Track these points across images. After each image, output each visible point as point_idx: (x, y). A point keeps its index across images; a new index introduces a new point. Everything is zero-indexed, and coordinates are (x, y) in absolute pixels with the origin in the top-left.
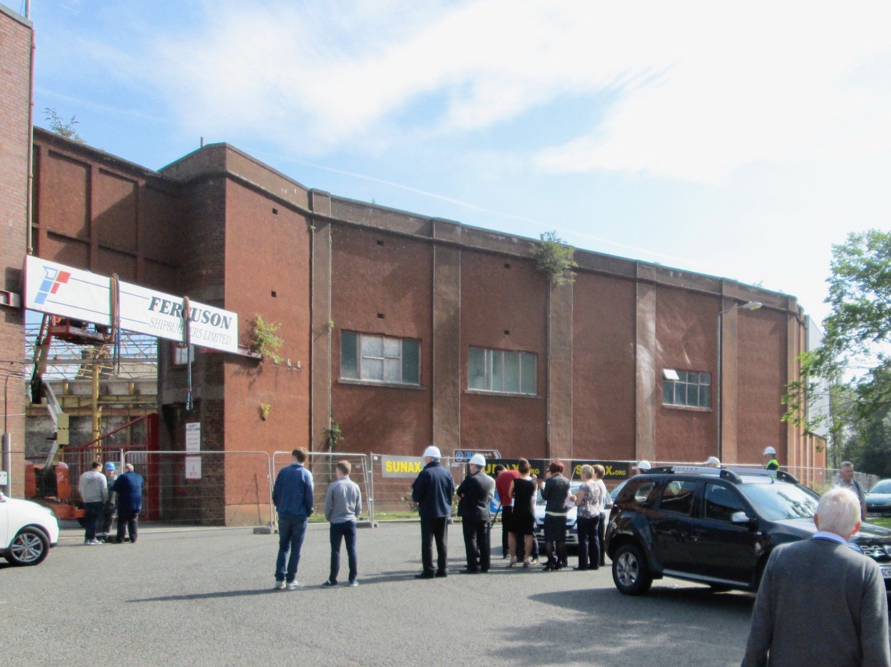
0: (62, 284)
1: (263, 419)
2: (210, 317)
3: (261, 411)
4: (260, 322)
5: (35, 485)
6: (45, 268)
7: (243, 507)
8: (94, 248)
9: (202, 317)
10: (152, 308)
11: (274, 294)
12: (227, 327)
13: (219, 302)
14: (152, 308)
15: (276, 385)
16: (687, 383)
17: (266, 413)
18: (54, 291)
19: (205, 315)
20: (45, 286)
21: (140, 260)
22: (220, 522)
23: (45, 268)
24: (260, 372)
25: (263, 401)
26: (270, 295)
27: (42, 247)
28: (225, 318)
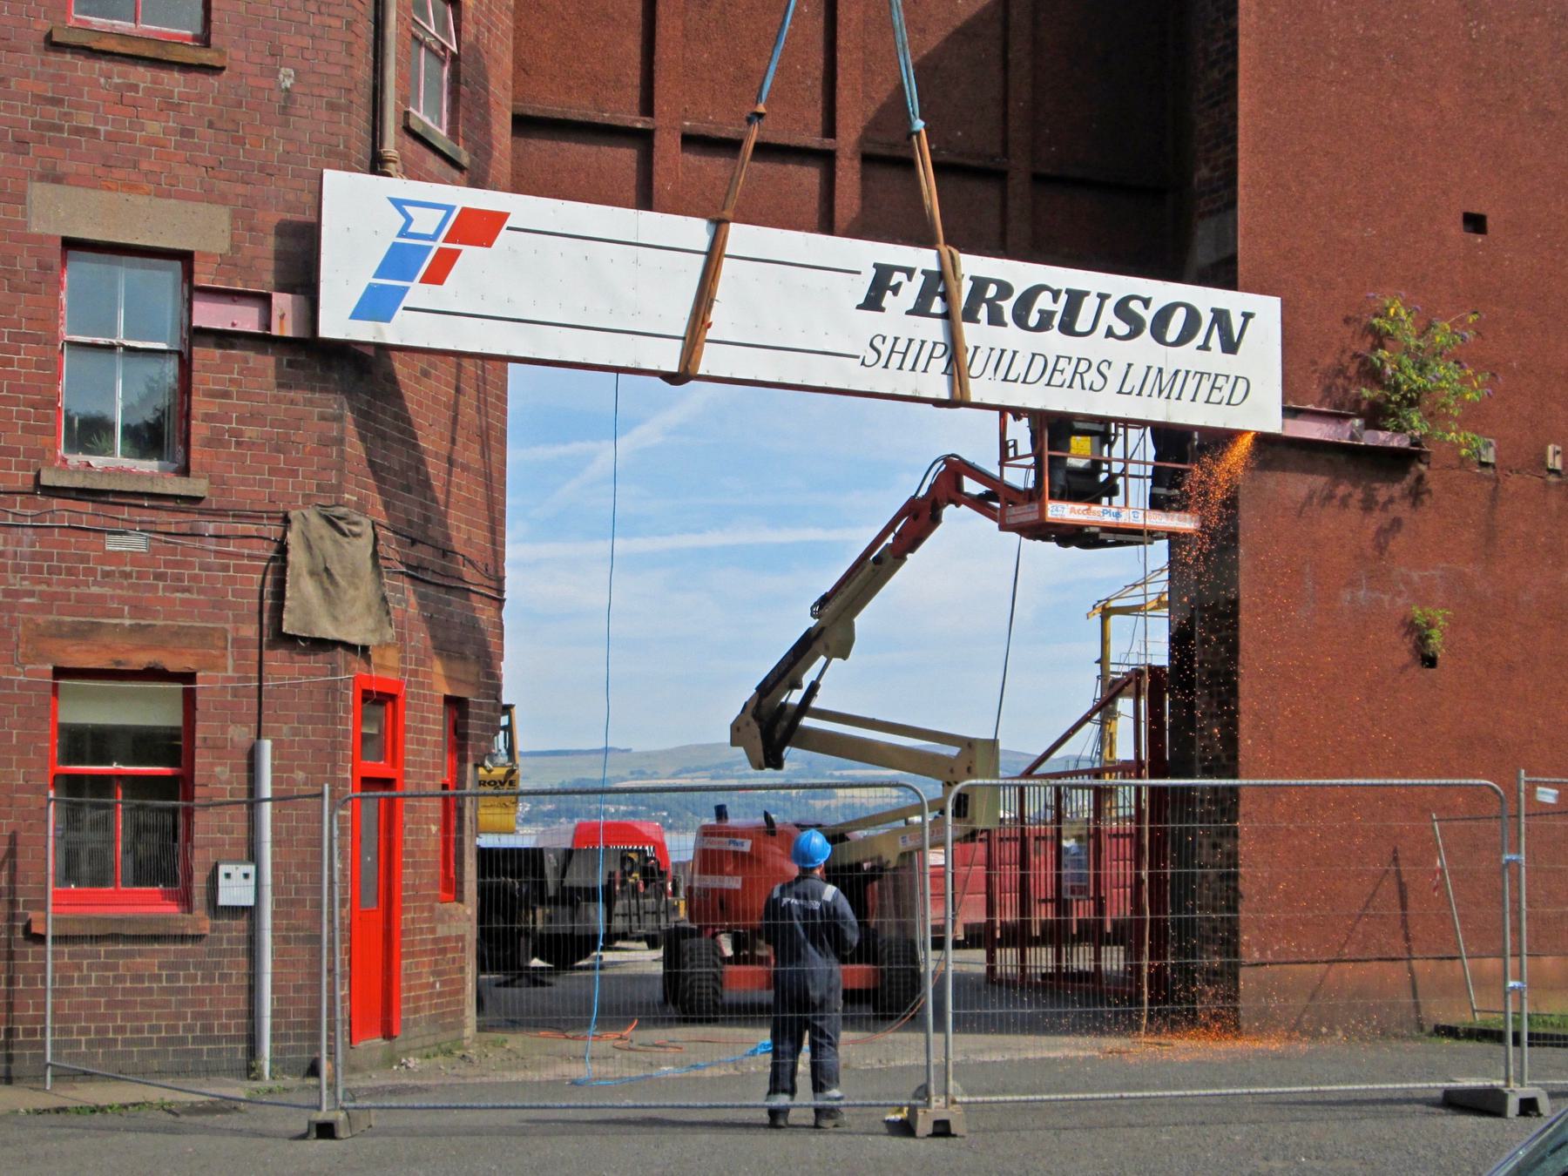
0: (469, 252)
1: (1430, 662)
2: (1148, 316)
3: (1418, 635)
4: (1398, 313)
5: (668, 843)
6: (399, 204)
7: (1349, 972)
8: (667, 146)
9: (1109, 317)
10: (873, 302)
11: (1475, 223)
12: (1230, 346)
13: (1223, 275)
14: (873, 302)
15: (1490, 535)
16: (1170, 961)
17: (1436, 640)
18: (436, 275)
19: (1122, 310)
20: (399, 262)
21: (1019, 182)
22: (1229, 1022)
23: (399, 204)
24: (1416, 494)
25: (1424, 602)
26: (1456, 230)
27: (662, 183)
28: (1221, 317)
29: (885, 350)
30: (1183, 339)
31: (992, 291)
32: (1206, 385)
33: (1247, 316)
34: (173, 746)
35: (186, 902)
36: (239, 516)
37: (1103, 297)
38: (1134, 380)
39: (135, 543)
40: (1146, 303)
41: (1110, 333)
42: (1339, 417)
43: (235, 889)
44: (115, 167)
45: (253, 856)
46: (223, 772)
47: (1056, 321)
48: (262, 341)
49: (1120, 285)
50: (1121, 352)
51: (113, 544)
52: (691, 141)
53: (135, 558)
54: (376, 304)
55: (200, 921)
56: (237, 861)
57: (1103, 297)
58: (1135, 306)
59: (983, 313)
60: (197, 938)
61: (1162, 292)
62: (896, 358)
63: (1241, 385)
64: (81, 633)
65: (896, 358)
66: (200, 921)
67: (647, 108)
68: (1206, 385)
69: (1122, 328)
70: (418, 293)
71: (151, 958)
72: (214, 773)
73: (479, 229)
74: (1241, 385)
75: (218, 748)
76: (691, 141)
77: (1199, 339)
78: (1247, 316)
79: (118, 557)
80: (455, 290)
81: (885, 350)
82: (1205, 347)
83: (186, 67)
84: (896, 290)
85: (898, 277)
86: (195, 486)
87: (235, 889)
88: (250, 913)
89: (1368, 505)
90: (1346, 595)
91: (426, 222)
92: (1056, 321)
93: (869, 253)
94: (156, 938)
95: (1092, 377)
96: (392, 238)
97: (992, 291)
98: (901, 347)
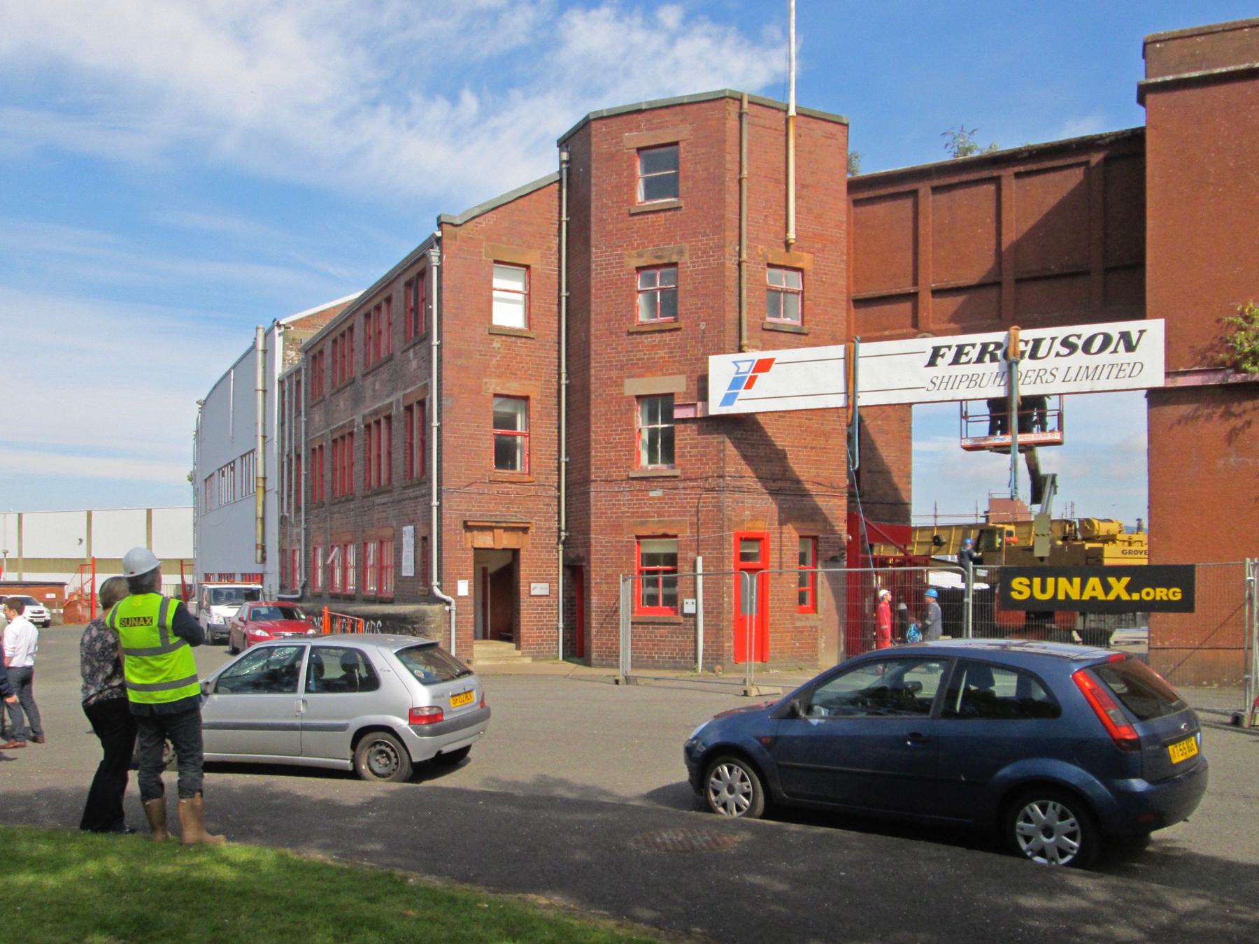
2: (1080, 343)
6: (735, 363)
10: (932, 363)
12: (1130, 348)
14: (932, 363)
18: (749, 386)
19: (1065, 343)
20: (736, 384)
23: (735, 363)
28: (1125, 336)
29: (938, 383)
30: (1103, 348)
31: (991, 348)
32: (1115, 370)
33: (1141, 332)
34: (672, 559)
35: (676, 613)
36: (690, 480)
37: (1053, 339)
38: (1072, 374)
39: (658, 493)
40: (1079, 337)
41: (1058, 354)
42: (1216, 371)
43: (689, 607)
44: (649, 368)
45: (695, 597)
46: (686, 568)
47: (1027, 355)
48: (694, 420)
49: (1061, 332)
50: (1063, 363)
51: (652, 494)
52: (936, 293)
53: (659, 499)
54: (729, 399)
55: (682, 620)
56: (689, 597)
57: (1053, 339)
58: (1072, 340)
59: (987, 357)
60: (679, 624)
61: (1086, 330)
62: (944, 385)
63: (1138, 367)
64: (643, 524)
65: (944, 385)
66: (682, 620)
67: (915, 283)
68: (1115, 370)
69: (1065, 351)
70: (743, 393)
71: (664, 630)
72: (684, 568)
73: (764, 366)
74: (1138, 367)
75: (685, 560)
76: (936, 293)
77: (1112, 348)
78: (1141, 332)
79: (653, 498)
80: (756, 390)
81: (938, 383)
82: (1115, 351)
83: (670, 330)
84: (942, 356)
85: (942, 351)
86: (677, 472)
87: (689, 607)
88: (695, 616)
89: (1228, 414)
90: (1221, 463)
91: (745, 367)
92: (1027, 355)
93: (927, 344)
94: (665, 624)
95: (1048, 377)
96: (733, 375)
97: (991, 348)
98: (945, 380)
